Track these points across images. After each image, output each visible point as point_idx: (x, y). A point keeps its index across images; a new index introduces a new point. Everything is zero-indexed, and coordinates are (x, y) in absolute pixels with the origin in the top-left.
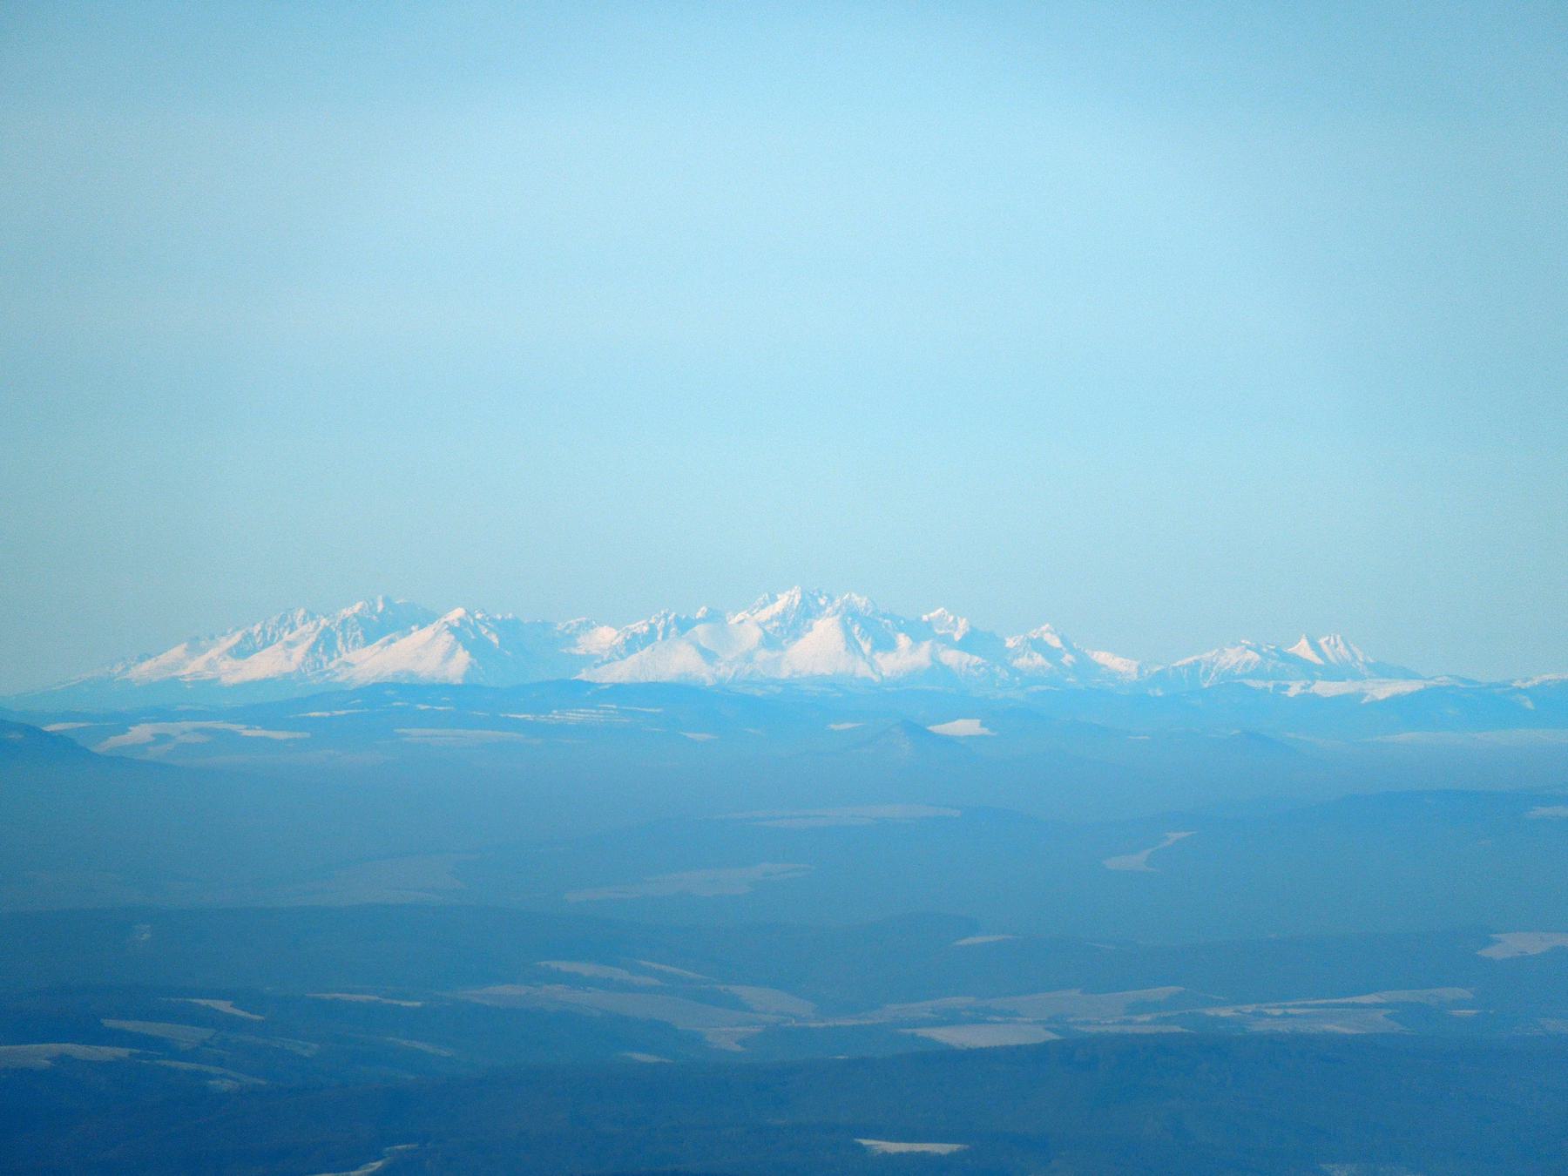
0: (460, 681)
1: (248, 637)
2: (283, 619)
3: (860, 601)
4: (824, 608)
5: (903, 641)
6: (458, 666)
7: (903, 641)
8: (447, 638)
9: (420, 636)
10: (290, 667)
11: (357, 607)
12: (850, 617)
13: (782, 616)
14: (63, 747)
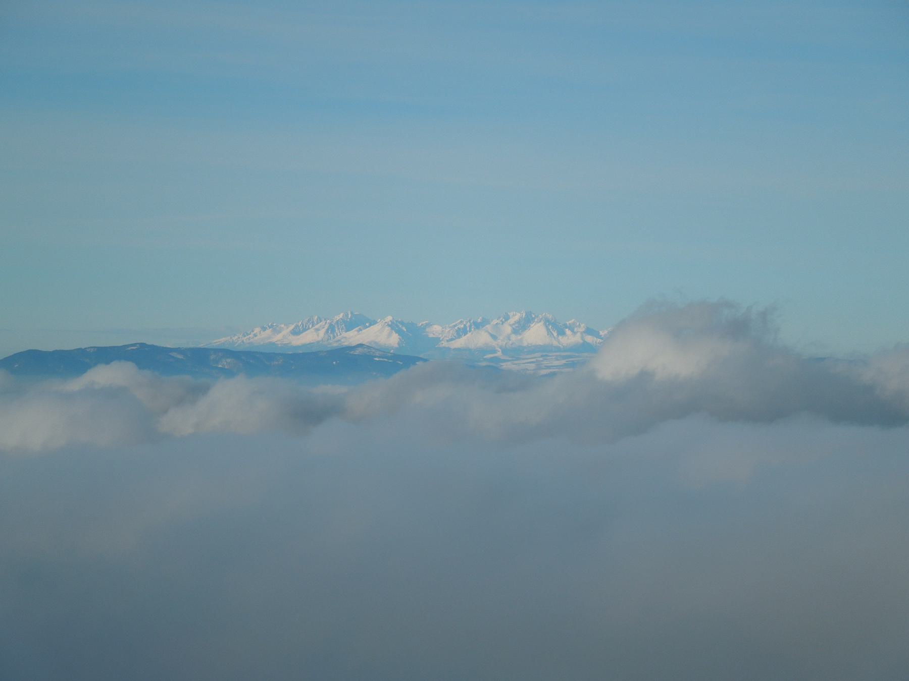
0: (396, 346)
1: (297, 326)
2: (309, 320)
3: (550, 316)
4: (534, 319)
5: (568, 332)
6: (394, 340)
7: (568, 332)
8: (387, 329)
9: (375, 328)
10: (320, 339)
11: (341, 315)
12: (547, 322)
13: (519, 322)
14: (822, 359)
